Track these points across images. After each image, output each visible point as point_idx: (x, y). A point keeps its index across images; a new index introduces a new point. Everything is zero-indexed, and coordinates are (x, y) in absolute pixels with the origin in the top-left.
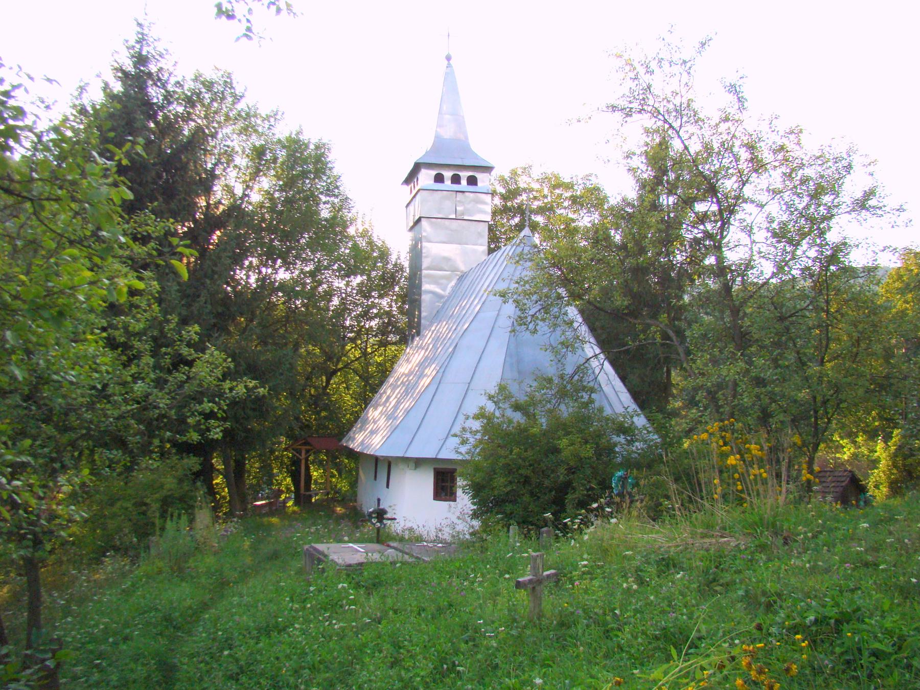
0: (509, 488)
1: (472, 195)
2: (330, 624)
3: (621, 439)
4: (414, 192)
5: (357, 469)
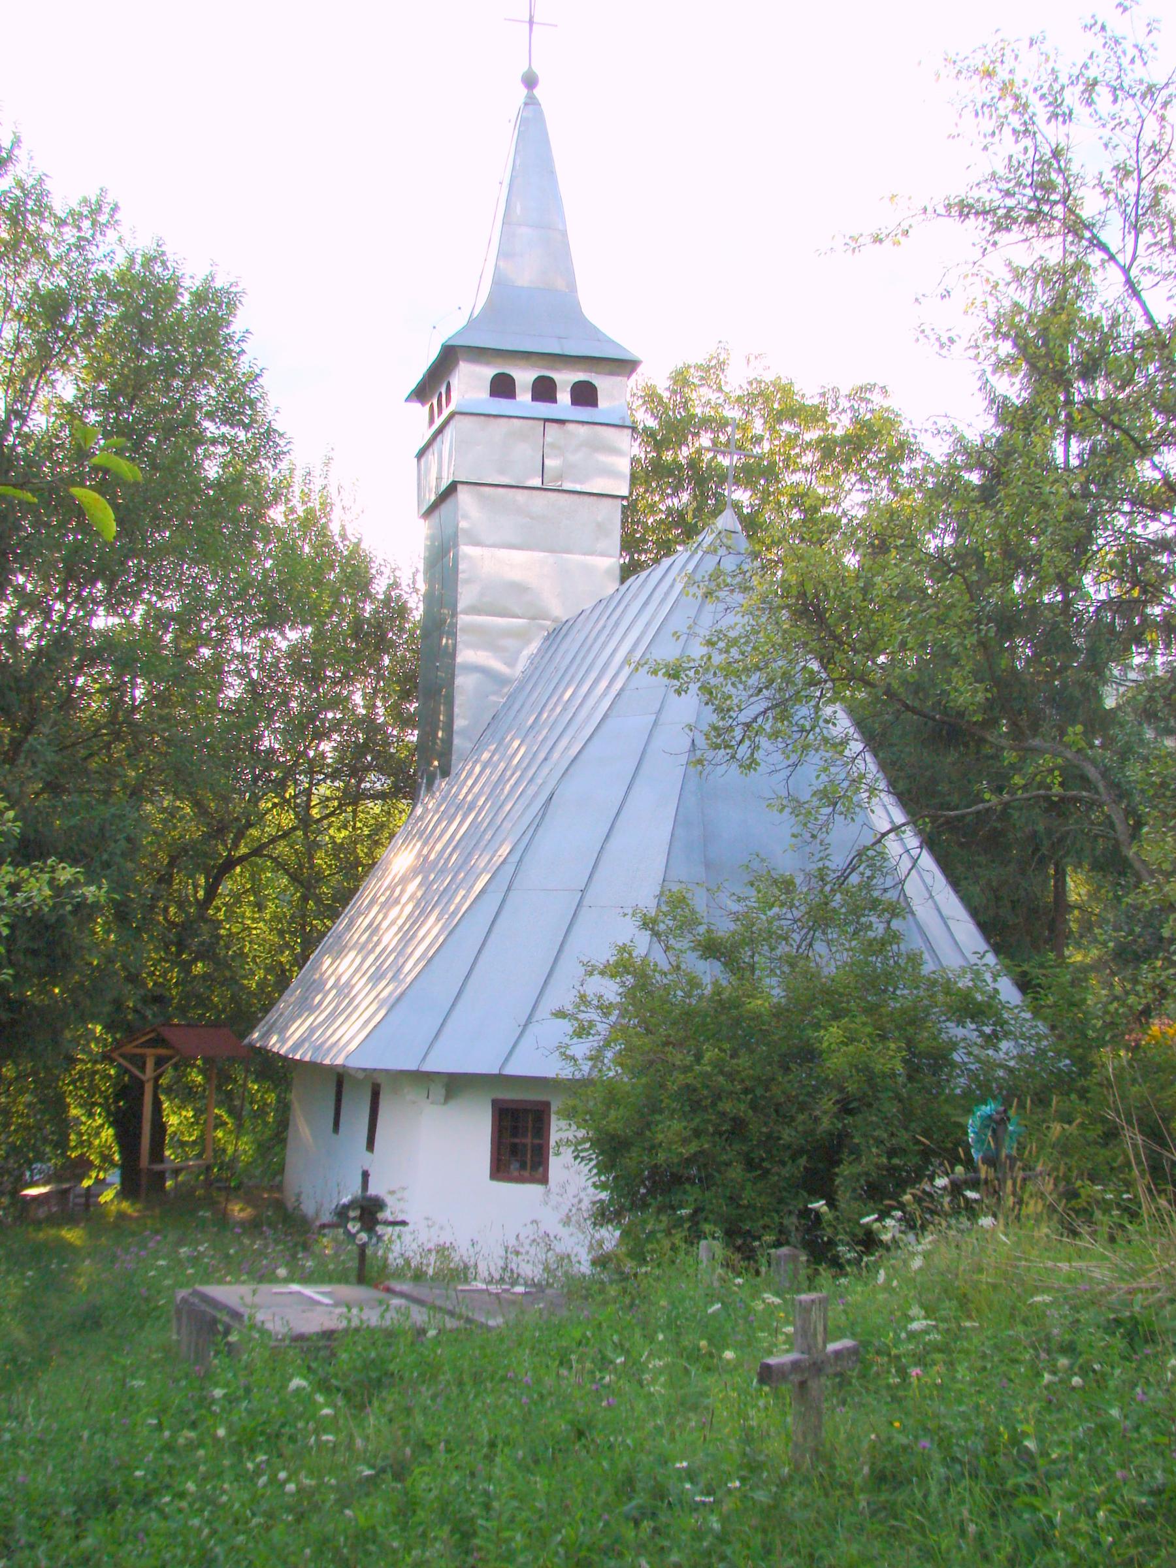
0: (693, 1148)
1: (583, 430)
2: (273, 1480)
3: (966, 1032)
4: (438, 422)
5: (284, 1108)
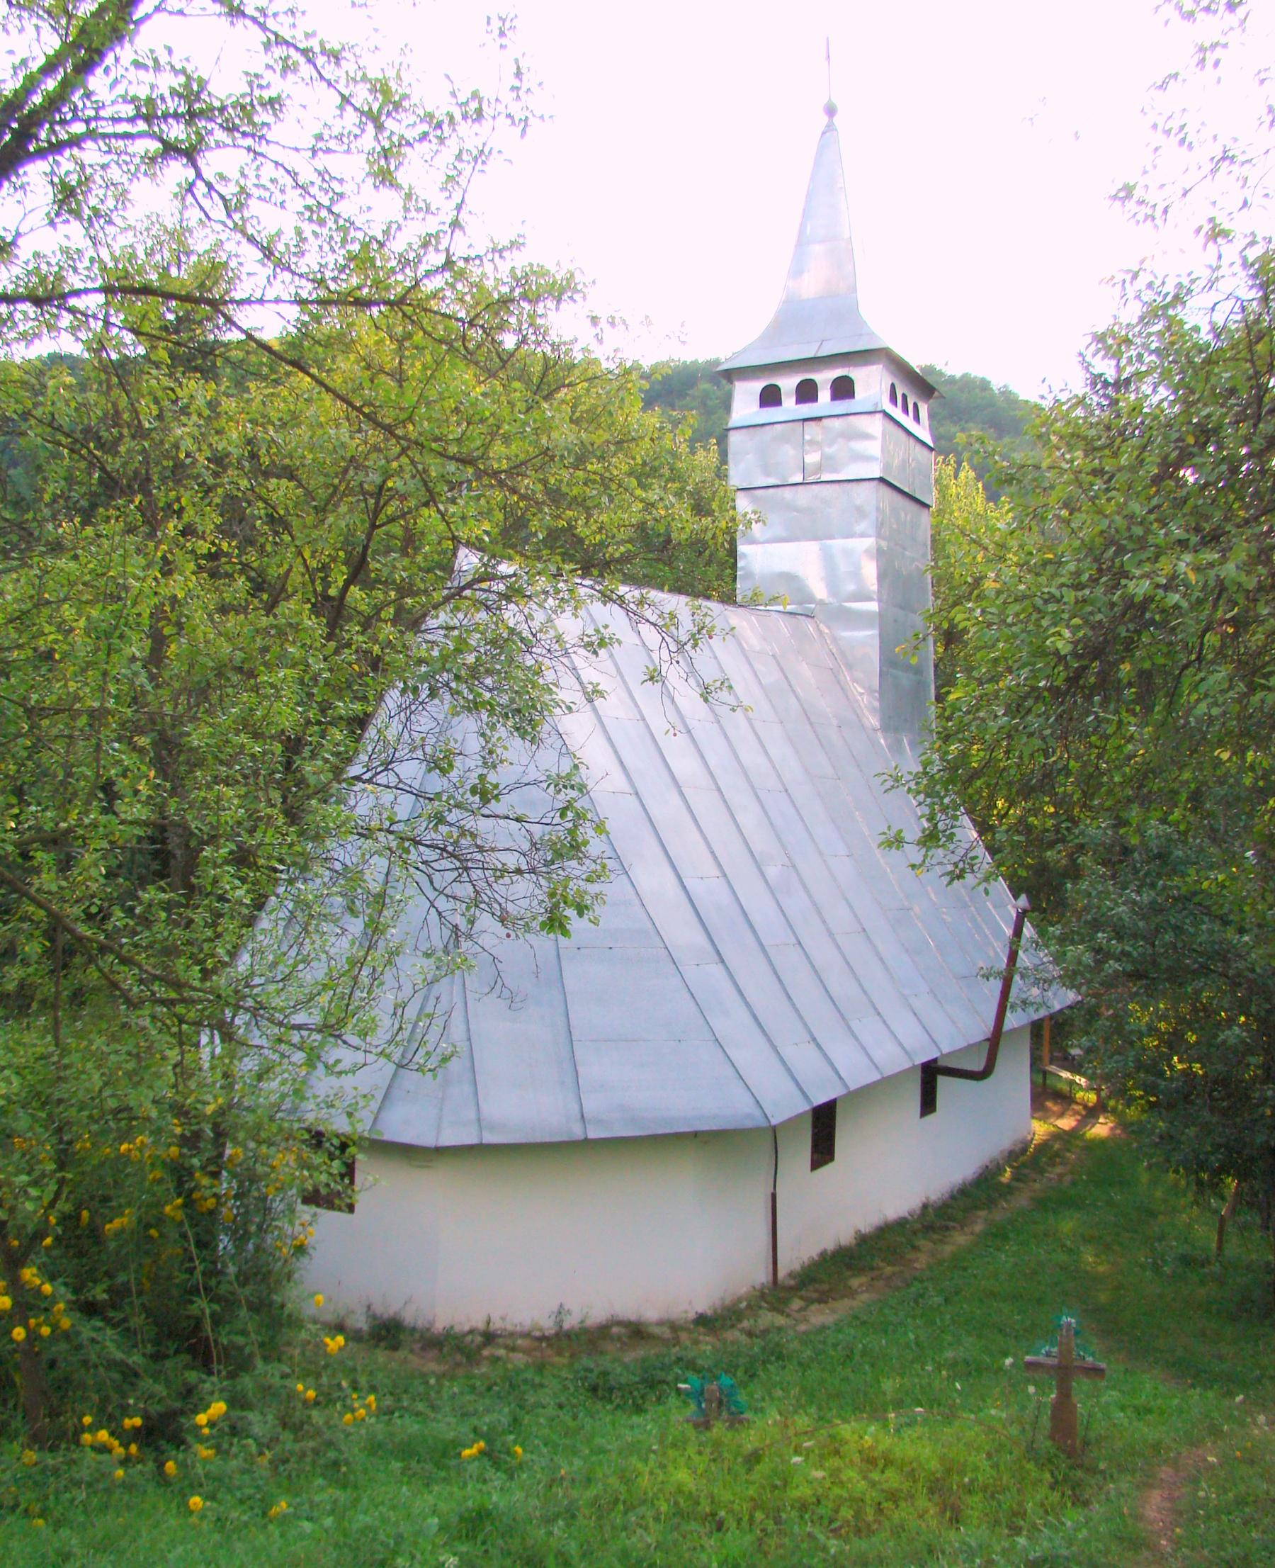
1: (837, 423)
